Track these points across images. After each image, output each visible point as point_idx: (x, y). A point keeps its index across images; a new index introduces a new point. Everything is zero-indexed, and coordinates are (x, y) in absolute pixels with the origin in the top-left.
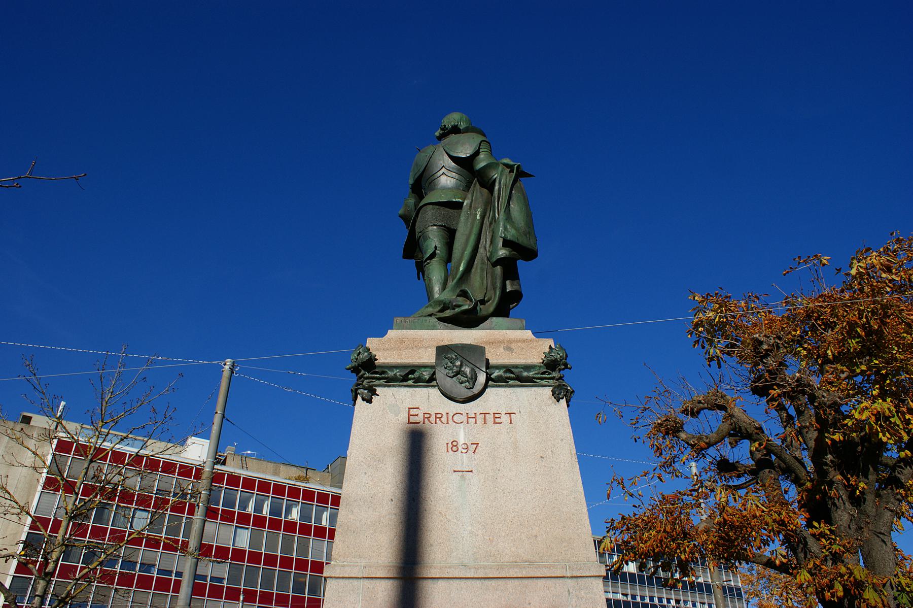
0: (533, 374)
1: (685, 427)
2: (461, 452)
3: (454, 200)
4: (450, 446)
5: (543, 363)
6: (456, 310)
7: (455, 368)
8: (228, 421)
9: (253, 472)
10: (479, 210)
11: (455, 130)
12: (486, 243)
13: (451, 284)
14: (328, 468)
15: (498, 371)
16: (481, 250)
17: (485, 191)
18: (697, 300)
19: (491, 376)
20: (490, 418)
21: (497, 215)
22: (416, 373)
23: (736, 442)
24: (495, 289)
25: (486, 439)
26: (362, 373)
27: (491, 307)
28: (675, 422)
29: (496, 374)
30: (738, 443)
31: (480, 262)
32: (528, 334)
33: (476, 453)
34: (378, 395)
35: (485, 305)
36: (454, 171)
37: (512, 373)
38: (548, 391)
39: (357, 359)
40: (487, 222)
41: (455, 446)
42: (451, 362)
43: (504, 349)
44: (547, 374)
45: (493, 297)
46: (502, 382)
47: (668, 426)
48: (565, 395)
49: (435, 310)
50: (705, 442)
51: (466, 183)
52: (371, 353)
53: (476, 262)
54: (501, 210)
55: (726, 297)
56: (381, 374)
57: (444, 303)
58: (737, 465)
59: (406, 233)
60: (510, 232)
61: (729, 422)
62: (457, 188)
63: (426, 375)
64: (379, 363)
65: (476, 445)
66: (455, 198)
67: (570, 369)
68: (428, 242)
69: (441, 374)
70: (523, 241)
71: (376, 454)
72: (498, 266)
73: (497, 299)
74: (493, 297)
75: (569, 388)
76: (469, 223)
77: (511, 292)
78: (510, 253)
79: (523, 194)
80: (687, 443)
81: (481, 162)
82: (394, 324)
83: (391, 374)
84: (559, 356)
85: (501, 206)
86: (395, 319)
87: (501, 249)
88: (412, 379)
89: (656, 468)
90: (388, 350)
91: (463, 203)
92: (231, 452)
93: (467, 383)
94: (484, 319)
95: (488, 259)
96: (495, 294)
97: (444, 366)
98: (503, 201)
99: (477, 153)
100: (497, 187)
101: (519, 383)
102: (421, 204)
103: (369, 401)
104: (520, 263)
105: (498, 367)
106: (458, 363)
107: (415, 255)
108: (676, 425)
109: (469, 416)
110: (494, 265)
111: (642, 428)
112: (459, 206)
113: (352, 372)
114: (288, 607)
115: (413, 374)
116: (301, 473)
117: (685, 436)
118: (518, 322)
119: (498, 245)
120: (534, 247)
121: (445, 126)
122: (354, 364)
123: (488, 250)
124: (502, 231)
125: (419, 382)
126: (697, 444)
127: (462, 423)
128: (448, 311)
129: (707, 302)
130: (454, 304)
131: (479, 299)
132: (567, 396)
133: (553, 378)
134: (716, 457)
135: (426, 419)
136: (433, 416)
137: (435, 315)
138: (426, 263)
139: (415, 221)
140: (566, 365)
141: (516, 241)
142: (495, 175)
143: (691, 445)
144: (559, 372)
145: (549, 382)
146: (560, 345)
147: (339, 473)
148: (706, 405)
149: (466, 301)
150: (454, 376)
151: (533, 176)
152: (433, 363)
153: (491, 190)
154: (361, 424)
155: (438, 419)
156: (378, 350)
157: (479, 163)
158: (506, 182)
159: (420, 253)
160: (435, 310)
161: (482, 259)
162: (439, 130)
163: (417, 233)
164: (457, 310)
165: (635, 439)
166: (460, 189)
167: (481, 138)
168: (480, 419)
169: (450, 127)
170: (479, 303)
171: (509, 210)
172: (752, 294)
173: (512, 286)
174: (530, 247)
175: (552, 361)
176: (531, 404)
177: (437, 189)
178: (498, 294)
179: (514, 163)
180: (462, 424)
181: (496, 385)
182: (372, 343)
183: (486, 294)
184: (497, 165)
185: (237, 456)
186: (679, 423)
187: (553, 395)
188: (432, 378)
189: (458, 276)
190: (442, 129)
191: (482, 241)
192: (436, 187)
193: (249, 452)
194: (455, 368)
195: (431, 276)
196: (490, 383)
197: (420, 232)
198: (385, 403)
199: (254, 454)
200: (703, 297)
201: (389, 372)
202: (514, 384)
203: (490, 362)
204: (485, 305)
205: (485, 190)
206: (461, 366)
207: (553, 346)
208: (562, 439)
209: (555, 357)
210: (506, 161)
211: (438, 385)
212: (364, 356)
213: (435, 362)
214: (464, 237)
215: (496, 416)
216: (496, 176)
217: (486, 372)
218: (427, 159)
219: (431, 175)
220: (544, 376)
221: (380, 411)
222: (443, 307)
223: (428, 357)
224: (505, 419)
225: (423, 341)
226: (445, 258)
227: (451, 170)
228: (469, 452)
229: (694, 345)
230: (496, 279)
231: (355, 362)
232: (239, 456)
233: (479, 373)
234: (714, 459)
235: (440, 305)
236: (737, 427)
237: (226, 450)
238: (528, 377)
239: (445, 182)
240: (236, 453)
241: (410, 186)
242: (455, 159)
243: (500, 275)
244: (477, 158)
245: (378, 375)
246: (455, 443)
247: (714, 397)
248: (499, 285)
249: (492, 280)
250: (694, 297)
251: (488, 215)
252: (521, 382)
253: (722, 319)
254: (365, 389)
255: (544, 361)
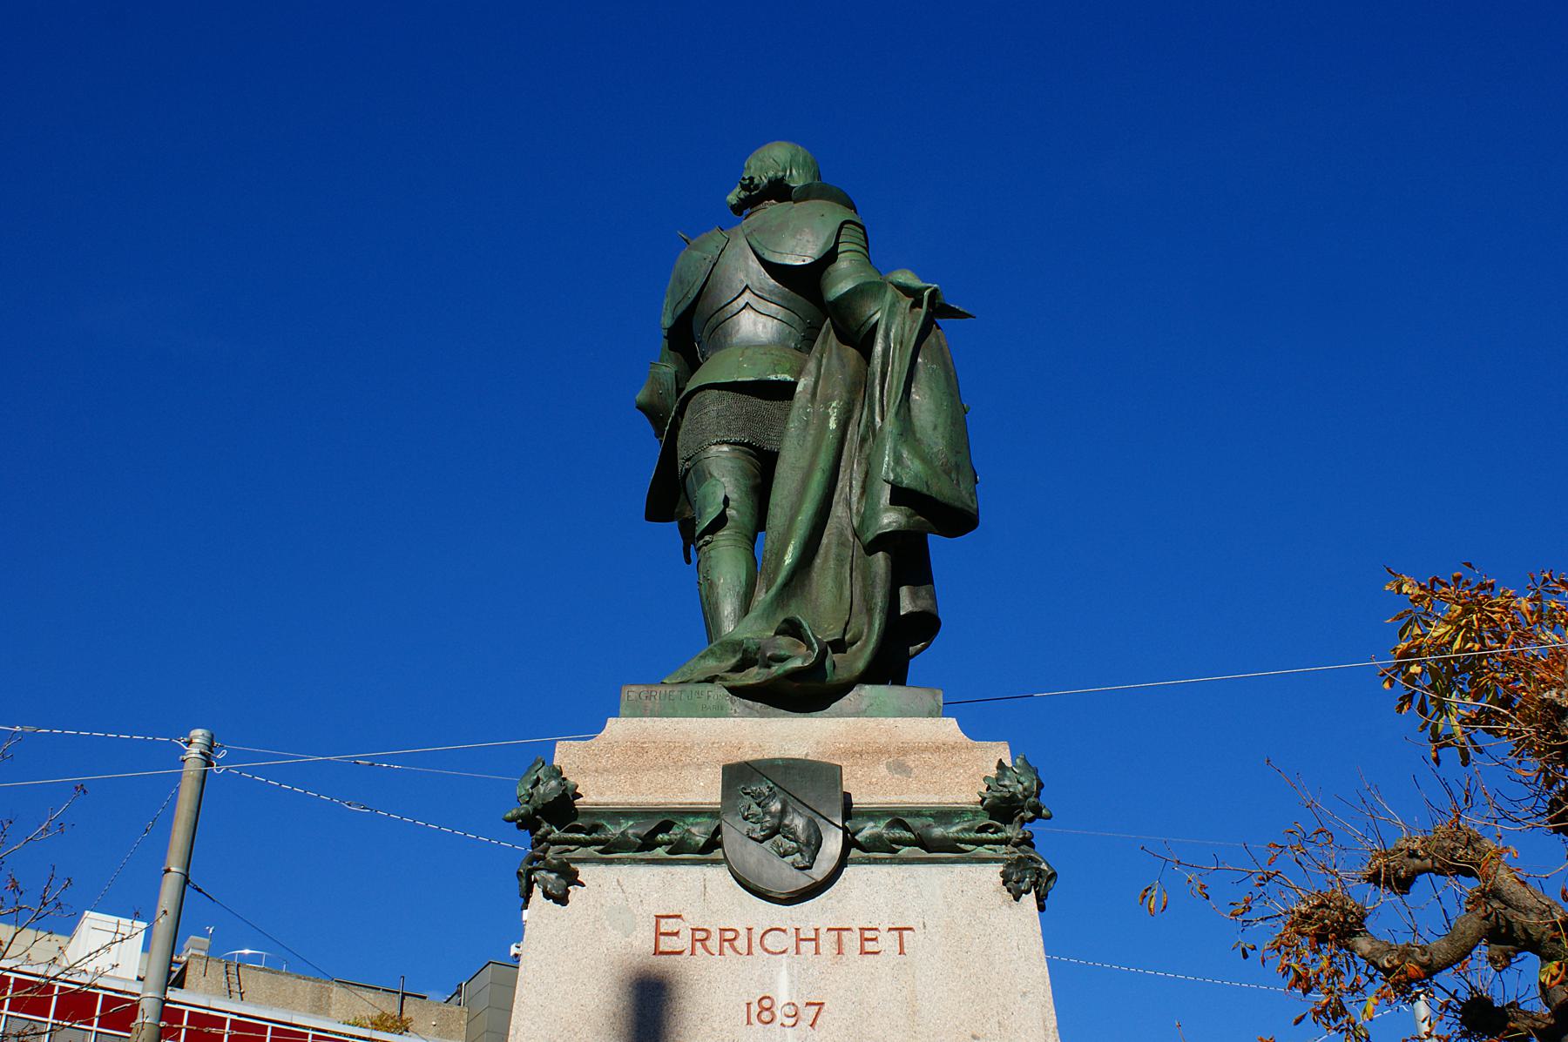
0: (957, 832)
1: (1368, 924)
2: (782, 1024)
3: (773, 378)
4: (755, 1009)
5: (982, 803)
6: (774, 669)
7: (768, 818)
8: (199, 890)
9: (258, 1004)
10: (834, 404)
11: (779, 190)
12: (850, 491)
13: (762, 597)
14: (459, 993)
15: (871, 824)
16: (838, 510)
17: (851, 352)
18: (1407, 593)
19: (856, 837)
20: (852, 941)
21: (878, 419)
22: (675, 830)
23: (1508, 958)
24: (870, 611)
25: (841, 992)
26: (543, 830)
27: (860, 657)
28: (1342, 909)
29: (868, 830)
30: (1513, 960)
31: (834, 540)
32: (949, 728)
33: (816, 1027)
34: (583, 885)
35: (845, 652)
36: (774, 298)
37: (907, 828)
38: (993, 872)
39: (531, 796)
40: (853, 435)
41: (767, 1009)
42: (759, 805)
43: (888, 767)
44: (991, 830)
45: (866, 630)
46: (882, 850)
47: (1326, 921)
48: (1035, 884)
49: (723, 665)
50: (1418, 963)
51: (804, 331)
52: (565, 779)
53: (825, 540)
54: (888, 406)
55: (1482, 587)
56: (588, 833)
57: (745, 651)
58: (1511, 1012)
59: (655, 449)
60: (908, 467)
61: (1480, 911)
62: (781, 343)
63: (699, 833)
64: (585, 803)
65: (817, 1008)
66: (776, 373)
67: (1049, 818)
68: (707, 488)
69: (733, 834)
70: (942, 489)
71: (577, 1030)
72: (880, 554)
73: (874, 638)
74: (866, 630)
75: (1043, 866)
76: (810, 438)
77: (910, 615)
78: (908, 522)
79: (945, 364)
80: (1375, 964)
81: (841, 281)
82: (623, 704)
83: (613, 831)
84: (1020, 787)
85: (889, 396)
86: (625, 690)
87: (886, 510)
88: (666, 844)
89: (1304, 1016)
90: (607, 770)
91: (795, 384)
92: (196, 952)
93: (798, 855)
94: (843, 689)
95: (856, 534)
96: (871, 624)
97: (743, 815)
98: (895, 383)
99: (830, 257)
100: (878, 348)
101: (923, 854)
102: (691, 386)
103: (562, 900)
104: (935, 542)
105: (872, 814)
106: (776, 806)
107: (677, 510)
108: (1345, 919)
109: (802, 936)
110: (871, 548)
111: (1261, 923)
112: (784, 391)
113: (519, 827)
114: (178, 1037)
115: (667, 832)
116: (390, 1005)
117: (1369, 947)
118: (926, 698)
119: (880, 498)
120: (969, 502)
121: (751, 179)
122: (525, 808)
123: (854, 511)
124: (888, 464)
125: (681, 851)
126: (1398, 967)
127: (784, 952)
128: (755, 670)
129: (1431, 600)
130: (768, 655)
131: (830, 639)
132: (1041, 886)
133: (1005, 842)
134: (1456, 991)
135: (698, 944)
136: (715, 936)
137: (722, 679)
138: (701, 542)
139: (676, 426)
140: (1037, 811)
141: (925, 490)
142: (876, 313)
143: (1384, 969)
144: (1021, 827)
145: (995, 851)
146: (1025, 759)
147: (489, 1007)
148: (1429, 861)
149: (799, 646)
150: (766, 838)
151: (970, 316)
152: (715, 804)
153: (866, 351)
154: (542, 957)
155: (726, 944)
156: (583, 772)
157: (835, 285)
158: (903, 335)
159: (689, 507)
160: (723, 665)
161: (841, 534)
162: (738, 189)
163: (680, 461)
164: (777, 669)
165: (1244, 950)
166: (788, 347)
167: (843, 214)
168: (828, 941)
169: (766, 181)
170: (829, 649)
171: (909, 409)
172: (1550, 575)
173: (914, 602)
174: (958, 504)
175: (1003, 799)
176: (950, 906)
177: (731, 346)
178: (877, 625)
179: (923, 285)
180: (784, 955)
181: (869, 859)
182: (568, 755)
183: (847, 624)
184: (881, 286)
185: (214, 964)
186: (1354, 914)
187: (1004, 883)
188: (714, 843)
189: (780, 580)
190: (744, 187)
191: (840, 485)
192: (729, 339)
193: (247, 951)
194: (768, 818)
195: (714, 575)
196: (855, 853)
197: (688, 460)
198: (599, 906)
199: (262, 955)
200: (1422, 588)
201: (608, 826)
202: (911, 856)
203: (854, 800)
204: (845, 652)
205: (851, 349)
206: (783, 812)
207: (1008, 762)
208: (1025, 993)
209: (1011, 790)
210: (906, 277)
211: (726, 860)
212: (549, 788)
213: (719, 800)
214: (798, 476)
215: (868, 934)
216: (878, 316)
217: (845, 830)
218: (707, 266)
219: (715, 308)
220: (984, 835)
221: (586, 924)
222: (741, 659)
223: (705, 790)
224: (887, 942)
225: (692, 747)
226: (750, 527)
227: (765, 295)
228: (800, 1023)
229: (1400, 708)
230: (873, 586)
231: (527, 802)
232: (220, 962)
233: (827, 830)
234: (1453, 996)
235: (735, 652)
236: (1502, 922)
237: (185, 946)
238: (944, 839)
239: (752, 328)
240: (213, 953)
241: (665, 333)
242: (775, 270)
243: (884, 576)
244: (830, 269)
245: (583, 835)
246: (766, 1003)
247: (1449, 841)
248: (879, 600)
249: (864, 586)
250: (1399, 587)
251: (856, 416)
252: (929, 852)
253: (1469, 645)
254: (550, 871)
255: (984, 799)
